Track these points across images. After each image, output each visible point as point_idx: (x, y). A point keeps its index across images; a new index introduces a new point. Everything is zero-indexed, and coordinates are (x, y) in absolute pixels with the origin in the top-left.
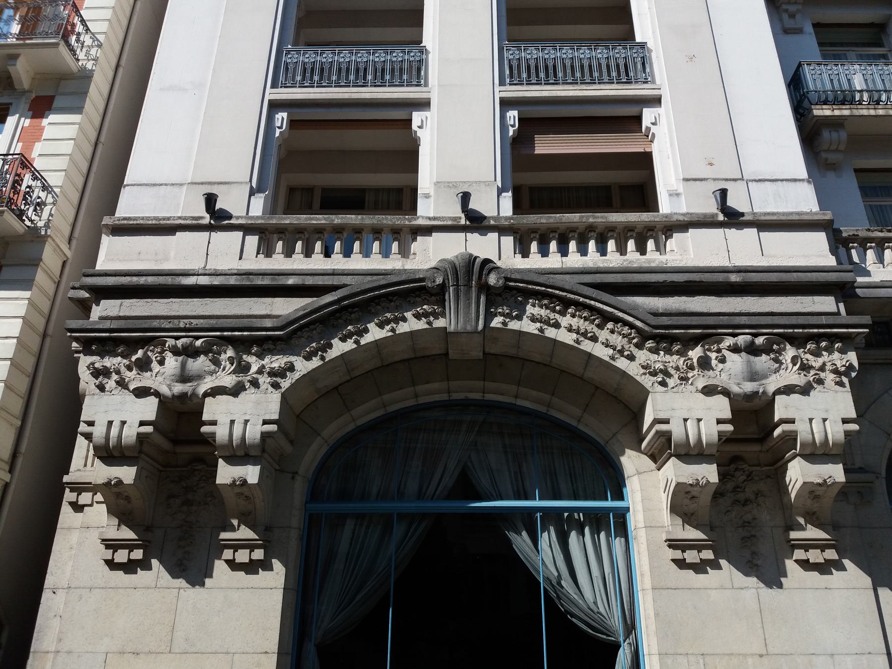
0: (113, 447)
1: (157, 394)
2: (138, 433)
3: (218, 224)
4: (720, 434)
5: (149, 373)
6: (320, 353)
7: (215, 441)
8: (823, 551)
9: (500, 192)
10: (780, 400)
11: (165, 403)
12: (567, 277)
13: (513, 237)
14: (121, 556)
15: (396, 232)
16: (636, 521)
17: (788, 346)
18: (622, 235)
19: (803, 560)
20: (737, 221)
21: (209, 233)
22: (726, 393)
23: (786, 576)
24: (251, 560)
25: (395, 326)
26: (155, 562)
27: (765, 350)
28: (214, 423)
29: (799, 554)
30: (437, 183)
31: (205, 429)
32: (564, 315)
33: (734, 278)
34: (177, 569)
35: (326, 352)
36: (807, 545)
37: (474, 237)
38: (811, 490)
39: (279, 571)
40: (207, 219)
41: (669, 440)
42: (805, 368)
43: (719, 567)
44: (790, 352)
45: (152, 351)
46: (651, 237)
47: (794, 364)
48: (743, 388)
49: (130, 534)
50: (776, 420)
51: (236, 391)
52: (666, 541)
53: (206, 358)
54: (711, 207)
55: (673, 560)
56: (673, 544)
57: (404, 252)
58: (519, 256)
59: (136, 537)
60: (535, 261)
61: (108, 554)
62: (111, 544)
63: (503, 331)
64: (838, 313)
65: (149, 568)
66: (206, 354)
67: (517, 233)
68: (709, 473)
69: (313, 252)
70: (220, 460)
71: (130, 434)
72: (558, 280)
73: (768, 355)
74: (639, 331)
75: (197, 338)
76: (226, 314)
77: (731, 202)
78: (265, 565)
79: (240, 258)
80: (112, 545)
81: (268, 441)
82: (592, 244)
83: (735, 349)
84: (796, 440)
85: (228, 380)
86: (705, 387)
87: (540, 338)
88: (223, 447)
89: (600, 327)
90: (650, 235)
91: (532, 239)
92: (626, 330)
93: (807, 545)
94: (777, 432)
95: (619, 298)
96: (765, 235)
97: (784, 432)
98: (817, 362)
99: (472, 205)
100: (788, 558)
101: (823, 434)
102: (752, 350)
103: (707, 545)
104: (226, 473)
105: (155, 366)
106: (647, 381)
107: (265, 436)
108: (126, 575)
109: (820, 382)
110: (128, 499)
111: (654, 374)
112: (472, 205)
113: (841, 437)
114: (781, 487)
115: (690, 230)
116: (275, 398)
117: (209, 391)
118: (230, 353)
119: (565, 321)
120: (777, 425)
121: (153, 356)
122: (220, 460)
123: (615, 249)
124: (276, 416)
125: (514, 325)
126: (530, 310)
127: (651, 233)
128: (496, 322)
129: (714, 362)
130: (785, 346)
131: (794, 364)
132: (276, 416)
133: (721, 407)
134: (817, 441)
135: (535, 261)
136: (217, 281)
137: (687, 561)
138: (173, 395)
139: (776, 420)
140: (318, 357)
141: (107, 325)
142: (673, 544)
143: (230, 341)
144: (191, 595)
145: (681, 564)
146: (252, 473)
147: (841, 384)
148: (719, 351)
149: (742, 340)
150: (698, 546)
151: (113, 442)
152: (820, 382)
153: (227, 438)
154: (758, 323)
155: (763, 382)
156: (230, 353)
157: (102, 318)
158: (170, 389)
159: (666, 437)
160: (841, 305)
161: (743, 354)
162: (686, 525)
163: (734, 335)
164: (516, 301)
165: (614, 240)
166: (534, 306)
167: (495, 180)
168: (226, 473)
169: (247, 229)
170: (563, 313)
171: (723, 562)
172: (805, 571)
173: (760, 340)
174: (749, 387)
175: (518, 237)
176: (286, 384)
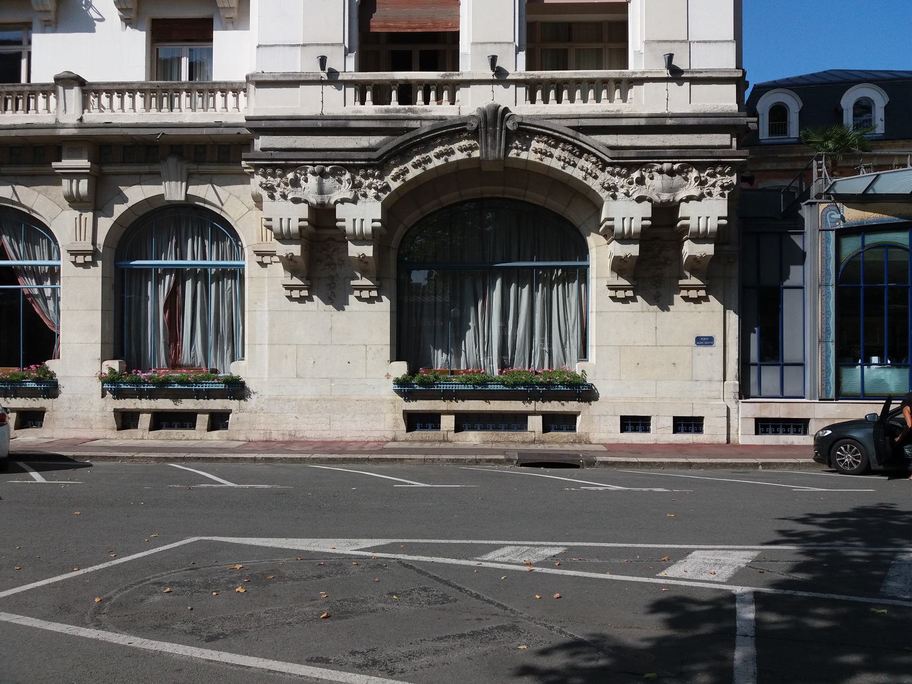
0: (285, 234)
1: (650, 200)
2: (299, 226)
3: (500, 79)
4: (719, 225)
5: (299, 189)
6: (402, 176)
7: (345, 231)
8: (625, 291)
9: (518, 50)
10: (339, 206)
11: (312, 209)
12: (556, 122)
13: (354, 89)
14: (621, 294)
15: (618, 82)
16: (592, 274)
17: (694, 170)
18: (599, 85)
19: (289, 296)
20: (679, 77)
21: (666, 83)
22: (650, 200)
23: (673, 304)
24: (626, 296)
25: (447, 157)
26: (315, 297)
27: (680, 172)
28: (343, 220)
29: (684, 293)
30: (473, 44)
31: (339, 224)
32: (556, 148)
33: (669, 122)
34: (328, 300)
35: (405, 175)
36: (688, 288)
37: (499, 88)
38: (692, 258)
39: (386, 303)
40: (666, 73)
41: (613, 230)
42: (702, 183)
43: (312, 300)
44: (694, 174)
45: (645, 171)
46: (605, 88)
47: (696, 182)
48: (303, 197)
49: (626, 283)
50: (679, 217)
51: (700, 198)
52: (607, 286)
53: (334, 180)
54: (314, 68)
55: (610, 297)
56: (611, 288)
57: (624, 98)
58: (358, 103)
59: (630, 284)
60: (540, 108)
61: (288, 293)
62: (696, 288)
63: (517, 160)
64: (730, 146)
65: (312, 300)
66: (680, 175)
67: (528, 84)
68: (633, 250)
69: (614, 100)
70: (349, 242)
71: (295, 226)
72: (554, 124)
73: (681, 175)
74: (603, 160)
75: (327, 165)
76: (654, 144)
77: (675, 62)
78: (379, 299)
79: (345, 106)
80: (289, 287)
81: (303, 231)
82: (552, 93)
83: (661, 172)
84: (689, 229)
85: (695, 191)
86: (293, 198)
87: (448, 164)
88: (350, 235)
89: (580, 157)
90: (566, 87)
91: (576, 88)
92: (594, 159)
93: (688, 288)
94: (679, 224)
95: (593, 137)
96: (695, 87)
97: (681, 225)
98: (711, 181)
99: (674, 62)
100: (677, 294)
101: (705, 226)
102: (671, 173)
103: (703, 287)
104: (689, 249)
105: (647, 180)
106: (604, 194)
107: (374, 229)
108: (327, 306)
109: (710, 194)
110: (296, 262)
111: (608, 189)
112: (674, 62)
113: (370, 230)
114: (680, 255)
115: (644, 84)
116: (378, 205)
117: (684, 198)
118: (348, 176)
119: (557, 152)
120: (680, 220)
121: (647, 175)
122: (349, 242)
123: (395, 100)
124: (650, 215)
125: (524, 155)
126: (534, 144)
127: (566, 85)
128: (513, 153)
129: (302, 182)
130: (692, 169)
131: (696, 182)
132: (380, 217)
133: (646, 209)
134: (701, 231)
135: (540, 108)
136: (702, 121)
137: (293, 297)
138: (661, 202)
139: (679, 217)
140: (401, 180)
141: (265, 155)
142: (611, 288)
143: (348, 168)
144: (337, 314)
145: (614, 299)
146: (708, 249)
147: (722, 195)
148: (651, 172)
149: (666, 166)
150: (625, 289)
151: (285, 230)
152: (710, 194)
153: (280, 231)
154: (289, 153)
155: (329, 195)
156: (348, 176)
157: (263, 150)
158: (659, 197)
159: (611, 228)
160: (734, 140)
161: (665, 176)
162: (619, 277)
163: (661, 163)
164: (526, 138)
165: (567, 90)
166: (538, 142)
167: (514, 41)
168: (354, 251)
169: (518, 83)
170: (555, 147)
171: (639, 297)
172: (686, 302)
173: (676, 167)
174: (665, 197)
175: (529, 87)
176: (384, 196)
